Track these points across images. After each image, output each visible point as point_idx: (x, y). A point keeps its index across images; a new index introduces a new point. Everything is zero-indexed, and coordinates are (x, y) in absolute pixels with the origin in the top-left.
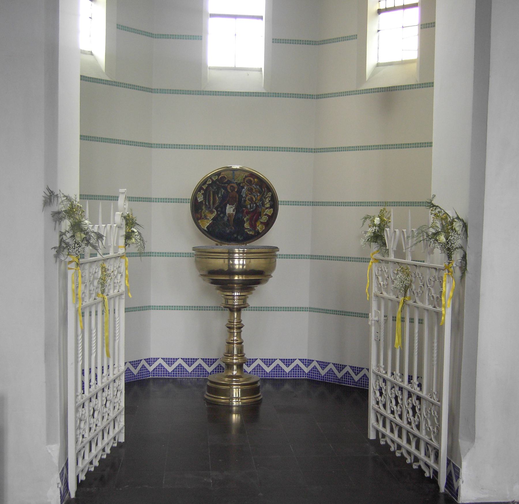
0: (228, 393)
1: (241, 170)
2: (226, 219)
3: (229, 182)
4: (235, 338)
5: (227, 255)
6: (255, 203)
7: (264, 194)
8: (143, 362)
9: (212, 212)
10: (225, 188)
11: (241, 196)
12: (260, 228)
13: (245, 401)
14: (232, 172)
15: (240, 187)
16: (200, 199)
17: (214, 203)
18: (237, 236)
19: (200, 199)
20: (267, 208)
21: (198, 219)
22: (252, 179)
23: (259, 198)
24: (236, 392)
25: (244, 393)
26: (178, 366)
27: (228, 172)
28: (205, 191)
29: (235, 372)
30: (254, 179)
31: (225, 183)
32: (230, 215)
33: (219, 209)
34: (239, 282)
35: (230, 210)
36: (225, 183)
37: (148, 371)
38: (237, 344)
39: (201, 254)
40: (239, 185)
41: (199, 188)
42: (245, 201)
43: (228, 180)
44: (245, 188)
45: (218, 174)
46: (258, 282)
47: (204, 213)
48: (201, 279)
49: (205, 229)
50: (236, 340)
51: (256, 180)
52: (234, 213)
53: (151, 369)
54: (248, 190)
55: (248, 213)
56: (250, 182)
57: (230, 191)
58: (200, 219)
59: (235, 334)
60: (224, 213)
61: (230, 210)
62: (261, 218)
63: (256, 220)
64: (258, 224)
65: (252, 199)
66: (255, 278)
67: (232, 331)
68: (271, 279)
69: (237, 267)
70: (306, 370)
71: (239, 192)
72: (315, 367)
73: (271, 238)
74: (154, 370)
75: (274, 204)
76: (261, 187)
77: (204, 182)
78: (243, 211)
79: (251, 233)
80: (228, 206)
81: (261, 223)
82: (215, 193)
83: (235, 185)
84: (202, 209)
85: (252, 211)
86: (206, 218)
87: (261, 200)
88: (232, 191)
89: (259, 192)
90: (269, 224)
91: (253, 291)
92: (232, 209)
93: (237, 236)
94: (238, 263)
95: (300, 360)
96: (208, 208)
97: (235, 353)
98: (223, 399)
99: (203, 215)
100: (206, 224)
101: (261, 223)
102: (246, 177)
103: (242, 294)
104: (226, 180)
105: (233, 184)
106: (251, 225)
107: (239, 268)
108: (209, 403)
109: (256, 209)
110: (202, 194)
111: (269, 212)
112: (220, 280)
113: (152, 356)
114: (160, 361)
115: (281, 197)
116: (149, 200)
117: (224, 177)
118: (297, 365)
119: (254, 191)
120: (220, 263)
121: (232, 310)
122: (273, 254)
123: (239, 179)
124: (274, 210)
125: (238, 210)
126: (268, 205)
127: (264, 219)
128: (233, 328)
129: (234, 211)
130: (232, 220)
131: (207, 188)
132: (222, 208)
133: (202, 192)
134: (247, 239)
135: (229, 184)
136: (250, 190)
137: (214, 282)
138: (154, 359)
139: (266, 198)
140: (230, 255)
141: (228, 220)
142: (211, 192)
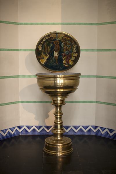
0: (56, 149)
1: (61, 33)
2: (54, 59)
3: (55, 40)
4: (59, 121)
5: (53, 78)
6: (68, 50)
7: (72, 46)
8: (17, 128)
9: (46, 56)
10: (53, 43)
11: (61, 47)
12: (71, 63)
13: (64, 153)
14: (56, 34)
15: (60, 42)
16: (40, 49)
17: (47, 51)
18: (60, 67)
19: (40, 49)
20: (74, 53)
21: (40, 59)
22: (66, 38)
23: (70, 48)
24: (60, 147)
25: (63, 149)
26: (33, 129)
27: (54, 35)
28: (43, 44)
29: (59, 138)
30: (67, 38)
31: (53, 40)
32: (56, 57)
33: (50, 54)
34: (60, 93)
35: (56, 54)
36: (53, 40)
37: (19, 132)
38: (60, 123)
39: (40, 78)
40: (60, 41)
41: (39, 43)
42: (63, 49)
43: (54, 39)
44: (63, 42)
45: (49, 35)
46: (70, 92)
47: (42, 56)
48: (40, 91)
49: (44, 64)
50: (60, 122)
51: (68, 38)
52: (58, 56)
53: (20, 131)
54: (64, 44)
55: (65, 56)
56: (65, 40)
57: (55, 44)
58: (41, 59)
59: (59, 119)
60: (53, 56)
61: (56, 54)
62: (72, 58)
63: (69, 60)
64: (70, 61)
65: (67, 48)
66: (70, 89)
67: (57, 117)
68: (76, 90)
69: (59, 84)
70: (95, 131)
71: (60, 45)
72: (99, 130)
73: (78, 68)
74: (22, 131)
75: (78, 51)
76: (71, 42)
77: (42, 40)
78: (62, 54)
79: (66, 66)
80: (55, 52)
81: (72, 60)
82: (48, 46)
83: (58, 41)
84: (42, 54)
85: (67, 54)
86: (43, 58)
87: (71, 49)
88: (56, 44)
89: (70, 45)
90: (76, 61)
91: (68, 97)
92: (57, 54)
93: (60, 67)
94: (60, 82)
95: (92, 126)
96: (44, 53)
97: (59, 128)
98: (53, 153)
99: (42, 57)
100: (43, 62)
101: (72, 60)
102: (63, 37)
103: (62, 98)
104: (53, 39)
105: (57, 41)
106: (66, 61)
107: (60, 85)
108: (46, 154)
109: (69, 54)
110: (41, 46)
111: (76, 55)
112: (50, 91)
113: (21, 125)
114: (25, 127)
115: (81, 48)
116: (98, 50)
117: (52, 37)
118: (90, 128)
119: (68, 44)
120: (50, 82)
121: (57, 106)
122: (77, 77)
123: (60, 38)
124: (78, 54)
125: (60, 54)
126: (75, 51)
127: (73, 58)
128: (58, 116)
129: (57, 55)
130: (57, 59)
131: (43, 43)
132: (51, 53)
133: (41, 45)
134: (63, 69)
135: (55, 41)
136: (66, 44)
137: (47, 92)
138: (22, 126)
139: (74, 48)
140: (55, 78)
141: (55, 59)
142: (46, 45)
